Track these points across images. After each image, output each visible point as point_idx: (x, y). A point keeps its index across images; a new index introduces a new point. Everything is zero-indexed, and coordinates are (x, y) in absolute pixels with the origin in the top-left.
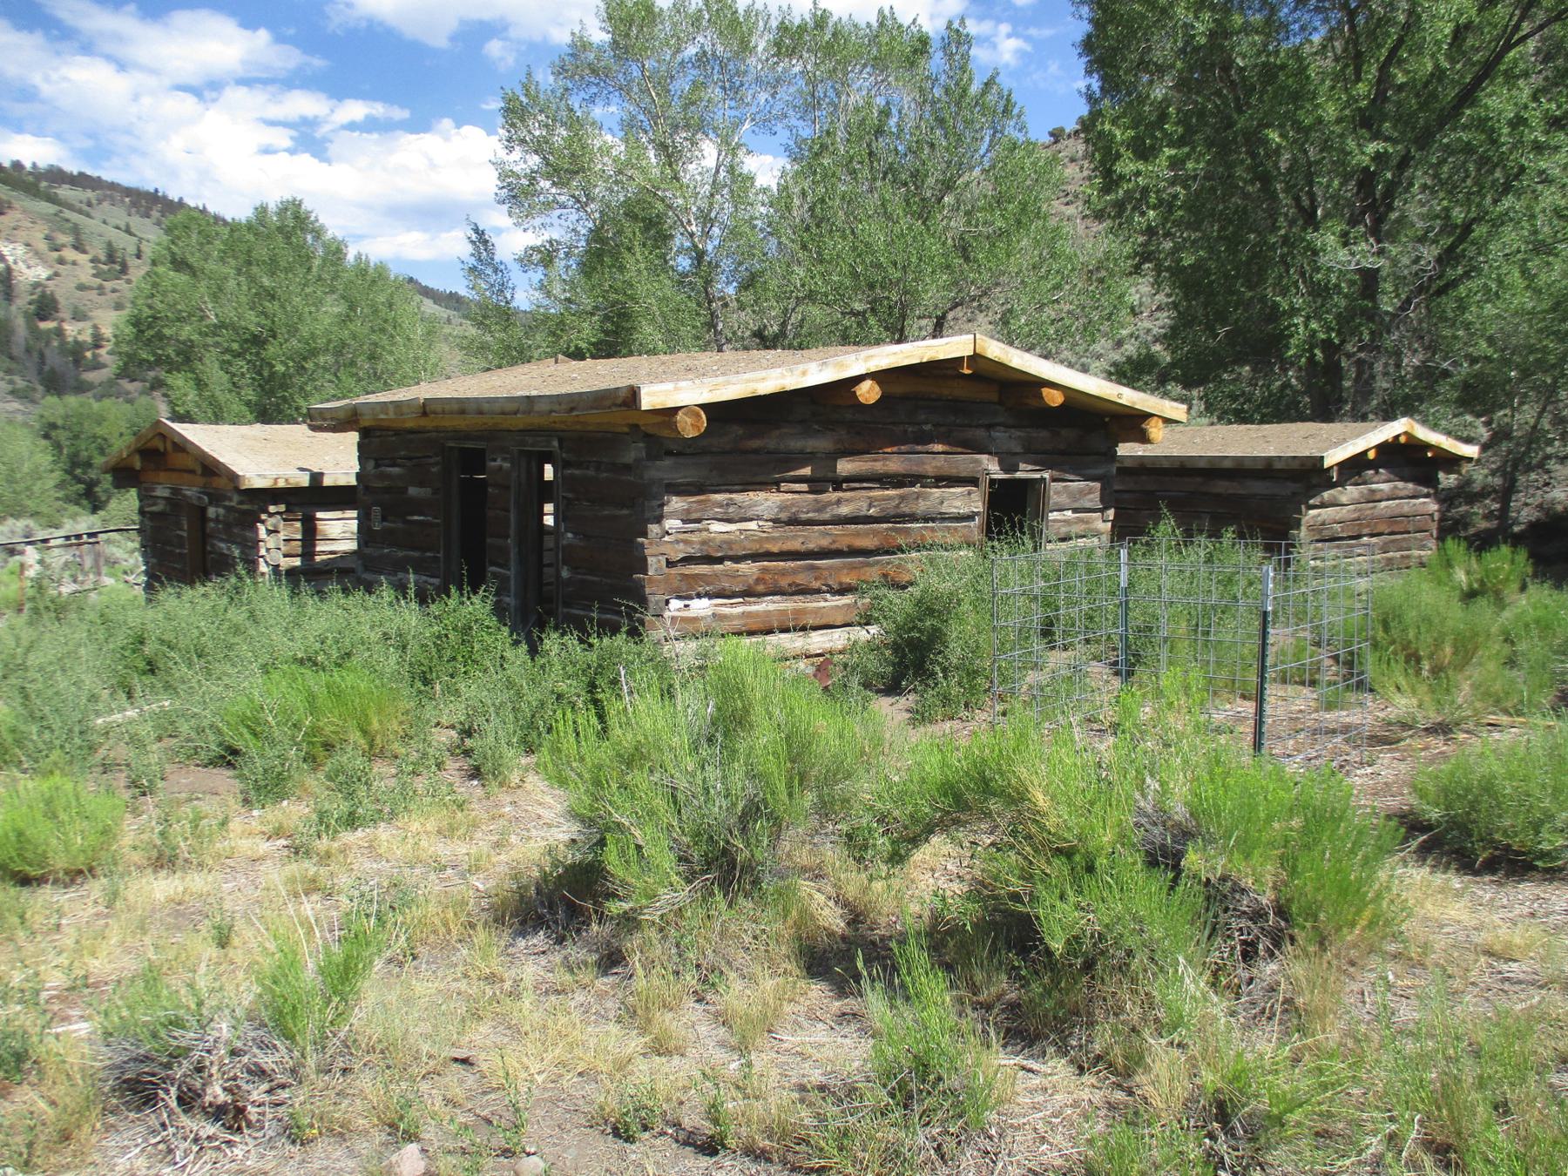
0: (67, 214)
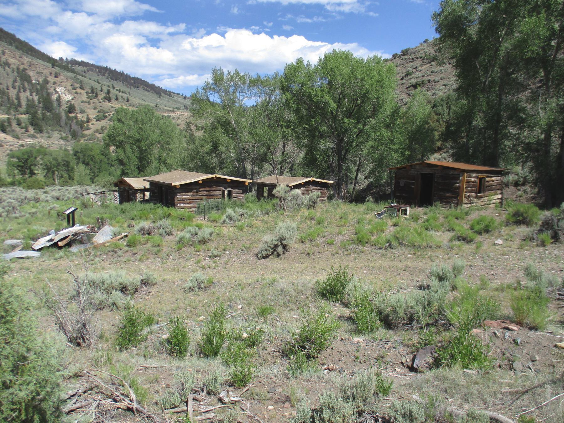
0: (78, 77)
